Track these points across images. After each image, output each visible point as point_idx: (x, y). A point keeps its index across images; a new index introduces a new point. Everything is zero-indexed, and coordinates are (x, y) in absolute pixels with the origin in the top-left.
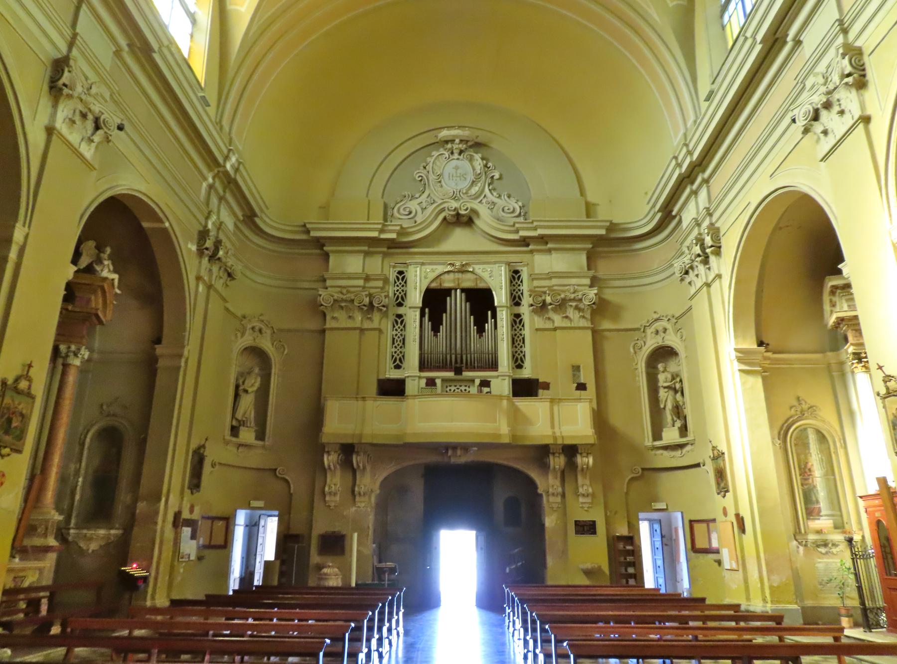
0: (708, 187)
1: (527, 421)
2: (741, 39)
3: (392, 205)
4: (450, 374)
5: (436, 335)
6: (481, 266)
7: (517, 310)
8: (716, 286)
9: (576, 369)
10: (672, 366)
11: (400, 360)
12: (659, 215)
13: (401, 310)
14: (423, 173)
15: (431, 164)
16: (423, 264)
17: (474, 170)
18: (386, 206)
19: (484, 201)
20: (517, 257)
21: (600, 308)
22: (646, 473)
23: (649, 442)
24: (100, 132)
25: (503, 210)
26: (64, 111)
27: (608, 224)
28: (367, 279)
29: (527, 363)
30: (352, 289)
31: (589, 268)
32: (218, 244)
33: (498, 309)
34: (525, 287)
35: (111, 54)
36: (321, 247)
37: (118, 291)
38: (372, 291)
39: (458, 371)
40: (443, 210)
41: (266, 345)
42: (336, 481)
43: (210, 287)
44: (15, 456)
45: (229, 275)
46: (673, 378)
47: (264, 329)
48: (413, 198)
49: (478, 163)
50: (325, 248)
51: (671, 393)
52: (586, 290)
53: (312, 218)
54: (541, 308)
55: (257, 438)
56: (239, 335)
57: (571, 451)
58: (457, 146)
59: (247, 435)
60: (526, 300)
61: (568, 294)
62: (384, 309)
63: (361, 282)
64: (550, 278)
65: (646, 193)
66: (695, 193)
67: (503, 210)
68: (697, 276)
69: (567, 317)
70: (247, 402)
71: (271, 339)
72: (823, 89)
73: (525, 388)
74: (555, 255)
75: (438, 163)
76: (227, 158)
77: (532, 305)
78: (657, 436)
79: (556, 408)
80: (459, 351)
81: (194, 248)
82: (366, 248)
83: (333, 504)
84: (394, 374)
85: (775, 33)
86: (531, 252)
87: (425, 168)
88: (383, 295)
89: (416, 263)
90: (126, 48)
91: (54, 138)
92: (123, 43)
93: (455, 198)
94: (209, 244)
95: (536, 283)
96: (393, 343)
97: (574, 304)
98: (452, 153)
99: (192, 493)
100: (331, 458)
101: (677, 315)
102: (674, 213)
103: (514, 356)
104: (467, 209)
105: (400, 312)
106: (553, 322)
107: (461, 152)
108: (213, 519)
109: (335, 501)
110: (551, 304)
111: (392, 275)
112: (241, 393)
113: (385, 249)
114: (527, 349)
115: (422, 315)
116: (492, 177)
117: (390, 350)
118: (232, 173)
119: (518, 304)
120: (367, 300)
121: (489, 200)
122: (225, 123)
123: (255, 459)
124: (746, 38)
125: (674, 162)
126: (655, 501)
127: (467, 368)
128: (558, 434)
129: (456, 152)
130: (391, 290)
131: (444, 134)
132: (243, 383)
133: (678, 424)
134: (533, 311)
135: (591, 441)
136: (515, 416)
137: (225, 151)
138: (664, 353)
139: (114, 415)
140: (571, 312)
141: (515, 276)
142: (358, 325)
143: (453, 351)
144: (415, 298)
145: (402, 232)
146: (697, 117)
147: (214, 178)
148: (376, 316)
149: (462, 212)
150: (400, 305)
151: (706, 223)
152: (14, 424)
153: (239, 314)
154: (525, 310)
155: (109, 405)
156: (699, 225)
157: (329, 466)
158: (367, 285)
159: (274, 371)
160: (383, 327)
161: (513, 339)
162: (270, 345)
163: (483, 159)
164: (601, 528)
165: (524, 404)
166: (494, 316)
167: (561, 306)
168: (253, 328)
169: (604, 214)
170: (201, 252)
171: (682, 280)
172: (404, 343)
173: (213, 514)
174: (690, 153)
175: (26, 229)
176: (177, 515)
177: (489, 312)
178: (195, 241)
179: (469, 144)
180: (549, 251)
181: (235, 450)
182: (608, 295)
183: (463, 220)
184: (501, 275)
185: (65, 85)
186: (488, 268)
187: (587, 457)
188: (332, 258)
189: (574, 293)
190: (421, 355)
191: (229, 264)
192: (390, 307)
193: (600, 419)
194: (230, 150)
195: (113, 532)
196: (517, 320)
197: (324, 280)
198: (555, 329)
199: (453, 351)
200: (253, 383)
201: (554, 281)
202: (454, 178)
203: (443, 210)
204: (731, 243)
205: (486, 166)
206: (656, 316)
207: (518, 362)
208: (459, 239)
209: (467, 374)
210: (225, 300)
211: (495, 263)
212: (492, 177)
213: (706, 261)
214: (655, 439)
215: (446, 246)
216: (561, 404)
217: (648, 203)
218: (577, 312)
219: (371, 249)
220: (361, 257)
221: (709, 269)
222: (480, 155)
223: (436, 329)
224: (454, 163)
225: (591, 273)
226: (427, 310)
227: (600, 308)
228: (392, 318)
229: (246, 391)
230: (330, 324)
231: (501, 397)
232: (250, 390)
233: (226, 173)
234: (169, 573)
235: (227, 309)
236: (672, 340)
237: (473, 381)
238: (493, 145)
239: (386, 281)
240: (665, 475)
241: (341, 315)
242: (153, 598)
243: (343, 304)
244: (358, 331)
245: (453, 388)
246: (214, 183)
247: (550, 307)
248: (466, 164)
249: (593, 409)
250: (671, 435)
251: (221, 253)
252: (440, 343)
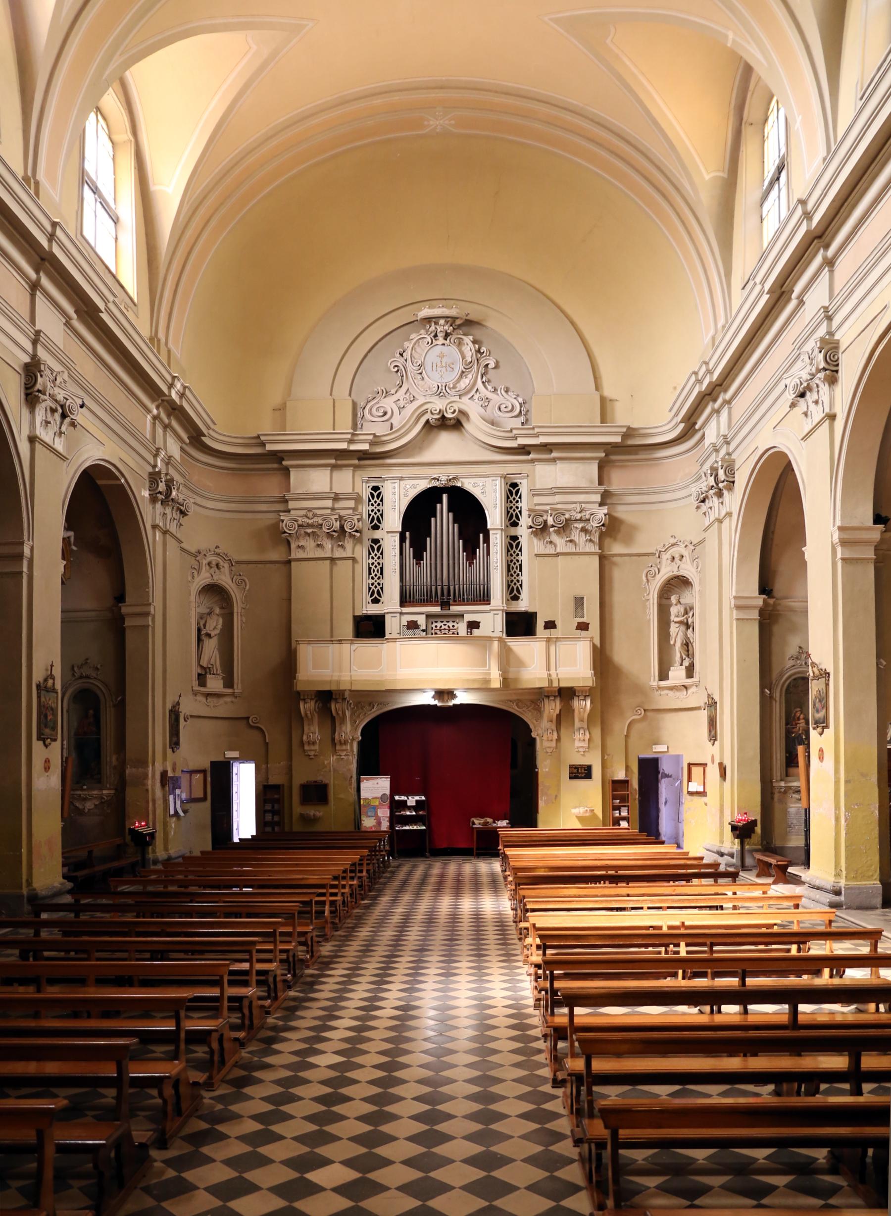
0: (730, 408)
1: (521, 664)
2: (751, 283)
3: (362, 404)
4: (437, 609)
5: (418, 564)
6: (472, 481)
7: (513, 531)
8: (726, 522)
9: (579, 602)
10: (687, 598)
11: (373, 496)
12: (682, 425)
13: (377, 534)
14: (400, 362)
15: (409, 351)
16: (401, 479)
17: (463, 357)
18: (354, 405)
19: (476, 397)
20: (515, 468)
21: (611, 528)
22: (649, 714)
23: (654, 683)
24: (67, 420)
25: (500, 409)
26: (40, 414)
27: (624, 430)
28: (336, 498)
29: (524, 594)
30: (319, 512)
31: (601, 482)
32: (169, 484)
33: (491, 532)
34: (524, 505)
35: (62, 326)
36: (278, 462)
37: (74, 548)
38: (342, 513)
39: (445, 605)
40: (425, 412)
41: (224, 579)
42: (314, 732)
43: (165, 532)
44: (53, 743)
45: (182, 512)
46: (686, 613)
47: (221, 563)
48: (387, 394)
49: (469, 349)
50: (284, 463)
51: (683, 628)
52: (595, 508)
53: (265, 427)
54: (541, 530)
55: (225, 686)
56: (196, 573)
57: (567, 694)
58: (443, 327)
59: (215, 684)
60: (525, 521)
61: (573, 513)
62: (358, 534)
63: (329, 503)
64: (554, 494)
65: (675, 388)
66: (718, 411)
67: (500, 409)
68: (711, 508)
69: (571, 541)
70: (211, 646)
71: (230, 573)
72: (808, 369)
73: (520, 624)
74: (560, 465)
75: (418, 350)
76: (171, 386)
77: (531, 527)
78: (663, 675)
79: (552, 648)
80: (445, 582)
81: (146, 494)
82: (333, 461)
83: (312, 753)
84: (373, 609)
85: (782, 287)
86: (532, 461)
87: (401, 355)
88: (356, 518)
89: (393, 478)
90: (74, 316)
91: (37, 445)
92: (70, 310)
93: (440, 392)
94: (162, 487)
95: (537, 500)
96: (370, 574)
97: (580, 525)
98: (436, 336)
99: (173, 752)
100: (307, 706)
101: (695, 542)
102: (697, 427)
103: (509, 586)
104: (455, 411)
105: (376, 537)
106: (556, 546)
107: (447, 335)
108: (192, 772)
109: (315, 750)
110: (553, 526)
111: (366, 492)
112: (203, 637)
113: (356, 462)
114: (525, 578)
115: (402, 540)
116: (487, 365)
117: (366, 581)
118: (177, 400)
119: (515, 524)
120: (337, 525)
121: (482, 395)
122: (161, 335)
123: (223, 708)
124: (755, 284)
125: (693, 378)
126: (657, 743)
127: (455, 601)
128: (554, 676)
129: (441, 335)
130: (365, 509)
131: (426, 312)
132: (205, 625)
133: (686, 663)
134: (532, 532)
135: (590, 683)
136: (507, 659)
137: (169, 379)
138: (679, 583)
139: (87, 677)
140: (576, 535)
141: (513, 489)
142: (328, 555)
143: (439, 582)
144: (393, 520)
145: (376, 441)
146: (727, 322)
147: (157, 408)
148: (349, 544)
149: (449, 415)
150: (376, 528)
151: (723, 452)
152: (49, 718)
153: (193, 550)
154: (523, 531)
155: (80, 667)
156: (717, 451)
157: (306, 714)
158: (336, 506)
159: (237, 609)
160: (357, 555)
161: (509, 566)
162: (230, 581)
163: (474, 342)
164: (597, 772)
165: (520, 645)
166: (487, 540)
167: (564, 528)
168: (209, 564)
169: (623, 417)
170: (153, 499)
171: (698, 508)
172: (382, 573)
173: (191, 768)
174: (709, 372)
175: (31, 542)
176: (164, 774)
177: (481, 535)
178: (147, 484)
179: (458, 322)
180: (554, 460)
181: (203, 699)
182: (621, 512)
183: (450, 424)
184: (495, 491)
185: (39, 391)
186: (480, 481)
187: (585, 700)
188: (293, 474)
189: (580, 512)
190: (402, 588)
191: (60, 398)
192: (365, 530)
193: (602, 660)
194: (174, 377)
195: (105, 792)
196: (513, 543)
197: (286, 501)
198: (557, 555)
199: (439, 582)
200: (215, 625)
201: (558, 498)
202: (436, 371)
203: (425, 412)
204: (742, 478)
205: (478, 351)
206: (673, 541)
207: (513, 593)
208: (445, 446)
209: (455, 609)
210: (180, 542)
211: (488, 476)
212: (487, 365)
213: (720, 494)
214: (661, 679)
215: (428, 456)
216: (558, 643)
217: (670, 411)
218: (583, 534)
219: (339, 462)
220: (327, 472)
221: (722, 503)
222: (471, 338)
223: (418, 556)
224: (438, 350)
225: (601, 489)
226: (408, 534)
227: (611, 528)
228: (367, 544)
229: (209, 636)
230: (296, 554)
231: (490, 639)
232: (213, 634)
233: (171, 402)
234: (175, 828)
235: (182, 549)
236: (687, 570)
237: (461, 616)
238: (488, 324)
239: (358, 499)
240: (669, 716)
241: (309, 543)
242: (166, 849)
243: (309, 531)
244: (328, 562)
245: (439, 624)
246: (39, 280)
247: (552, 530)
248: (453, 349)
249: (594, 646)
250: (677, 674)
251: (174, 493)
252: (423, 575)
